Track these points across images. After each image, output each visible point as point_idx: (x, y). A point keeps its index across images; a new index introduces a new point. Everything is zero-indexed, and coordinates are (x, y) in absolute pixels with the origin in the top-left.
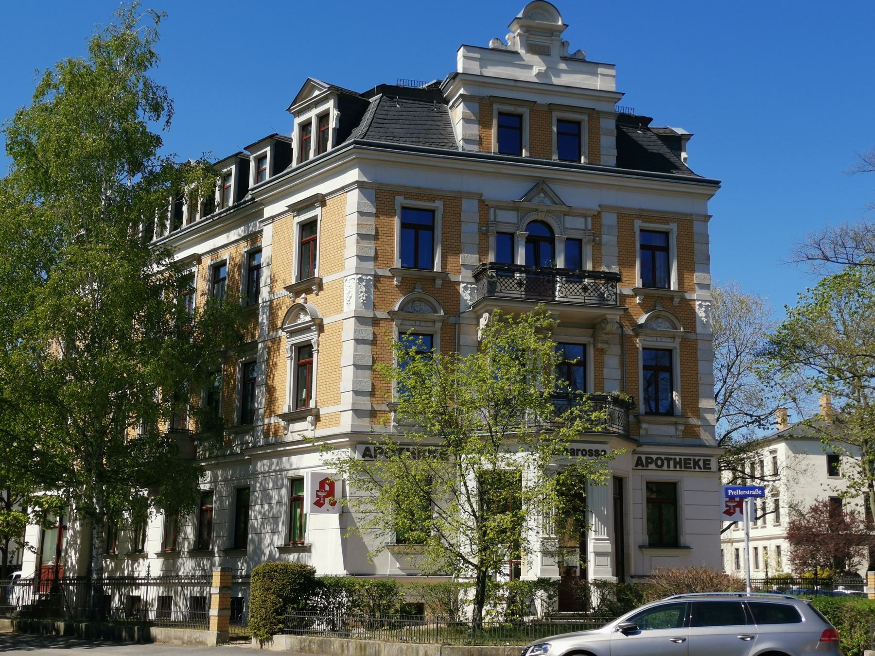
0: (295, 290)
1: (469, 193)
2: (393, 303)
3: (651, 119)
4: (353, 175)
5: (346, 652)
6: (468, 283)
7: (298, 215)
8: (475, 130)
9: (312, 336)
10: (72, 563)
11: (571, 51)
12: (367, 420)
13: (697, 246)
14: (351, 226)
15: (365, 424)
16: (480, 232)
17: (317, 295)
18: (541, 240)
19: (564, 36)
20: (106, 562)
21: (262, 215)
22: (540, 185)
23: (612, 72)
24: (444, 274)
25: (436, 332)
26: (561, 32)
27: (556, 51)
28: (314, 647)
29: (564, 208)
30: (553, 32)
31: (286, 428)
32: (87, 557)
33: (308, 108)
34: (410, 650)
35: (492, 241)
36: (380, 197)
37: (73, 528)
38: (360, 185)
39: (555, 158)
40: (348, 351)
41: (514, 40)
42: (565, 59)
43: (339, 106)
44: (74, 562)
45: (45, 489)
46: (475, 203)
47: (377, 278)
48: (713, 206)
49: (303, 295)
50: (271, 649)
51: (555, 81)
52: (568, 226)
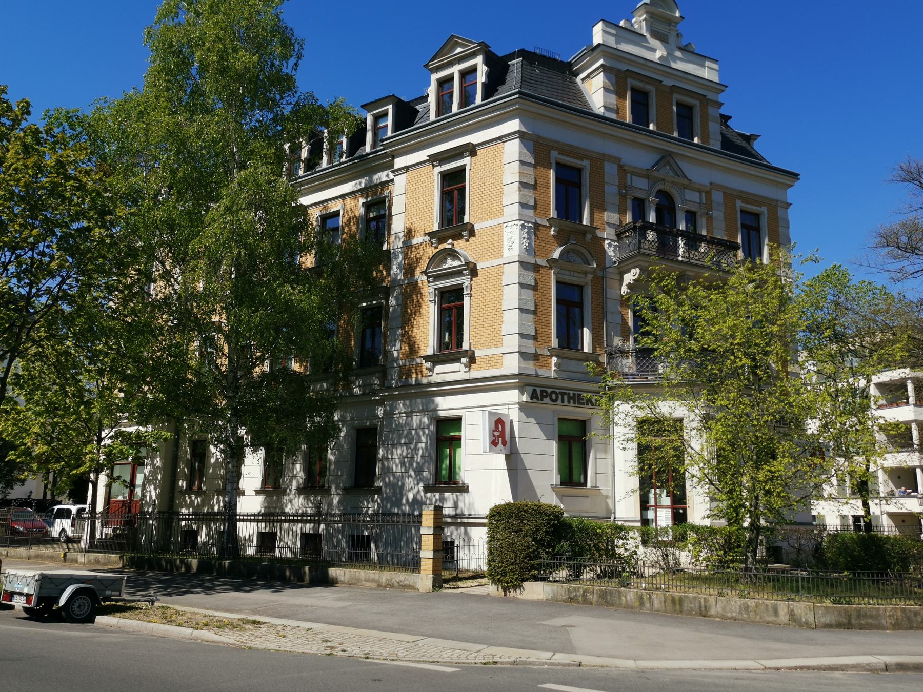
0: (436, 237)
1: (611, 156)
2: (551, 251)
3: (730, 117)
4: (514, 125)
5: (648, 605)
6: (612, 240)
7: (440, 165)
8: (613, 99)
9: (465, 281)
10: (151, 497)
11: (684, 42)
12: (532, 363)
13: (781, 229)
14: (511, 174)
15: (530, 367)
16: (620, 194)
17: (467, 240)
18: (666, 209)
19: (681, 27)
20: (190, 498)
21: (393, 166)
22: (666, 158)
23: (716, 66)
24: (592, 228)
25: (587, 284)
26: (677, 23)
27: (672, 39)
28: (594, 598)
29: (685, 182)
30: (670, 22)
31: (430, 370)
32: (170, 493)
33: (450, 64)
34: (762, 607)
35: (629, 203)
36: (538, 149)
37: (153, 464)
38: (521, 135)
39: (675, 135)
40: (511, 296)
41: (640, 22)
42: (681, 49)
43: (487, 62)
44: (154, 497)
45: (139, 424)
46: (615, 167)
47: (537, 226)
48: (792, 194)
49: (450, 241)
50: (519, 596)
51: (673, 65)
52: (687, 198)
